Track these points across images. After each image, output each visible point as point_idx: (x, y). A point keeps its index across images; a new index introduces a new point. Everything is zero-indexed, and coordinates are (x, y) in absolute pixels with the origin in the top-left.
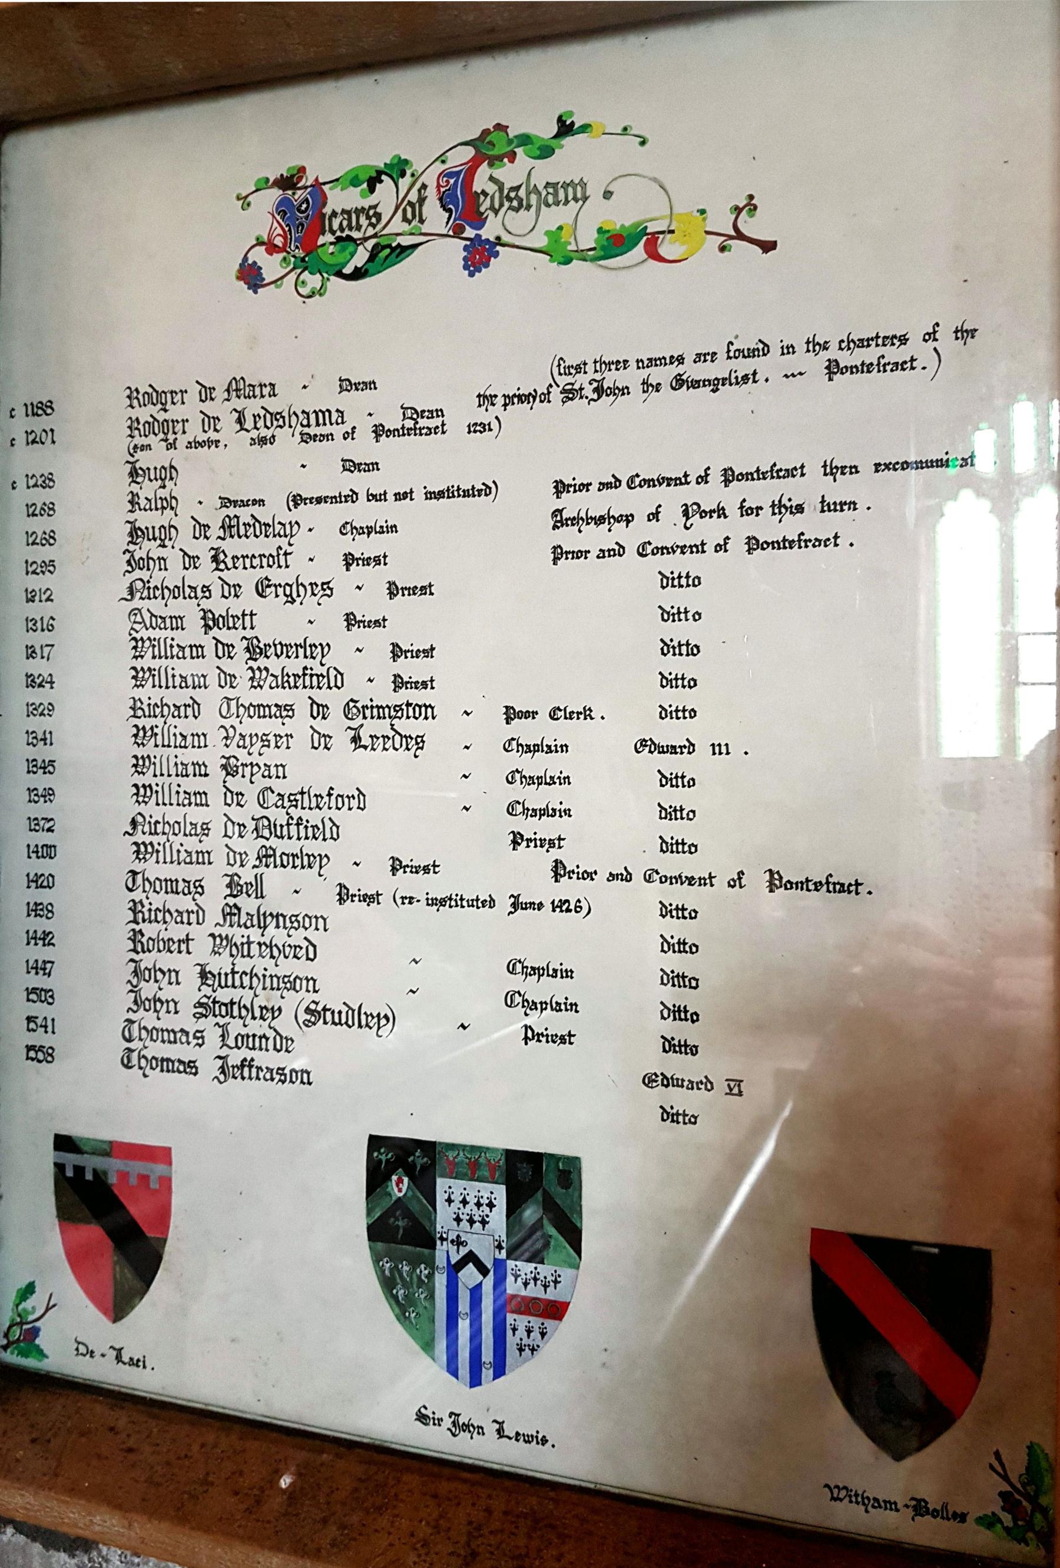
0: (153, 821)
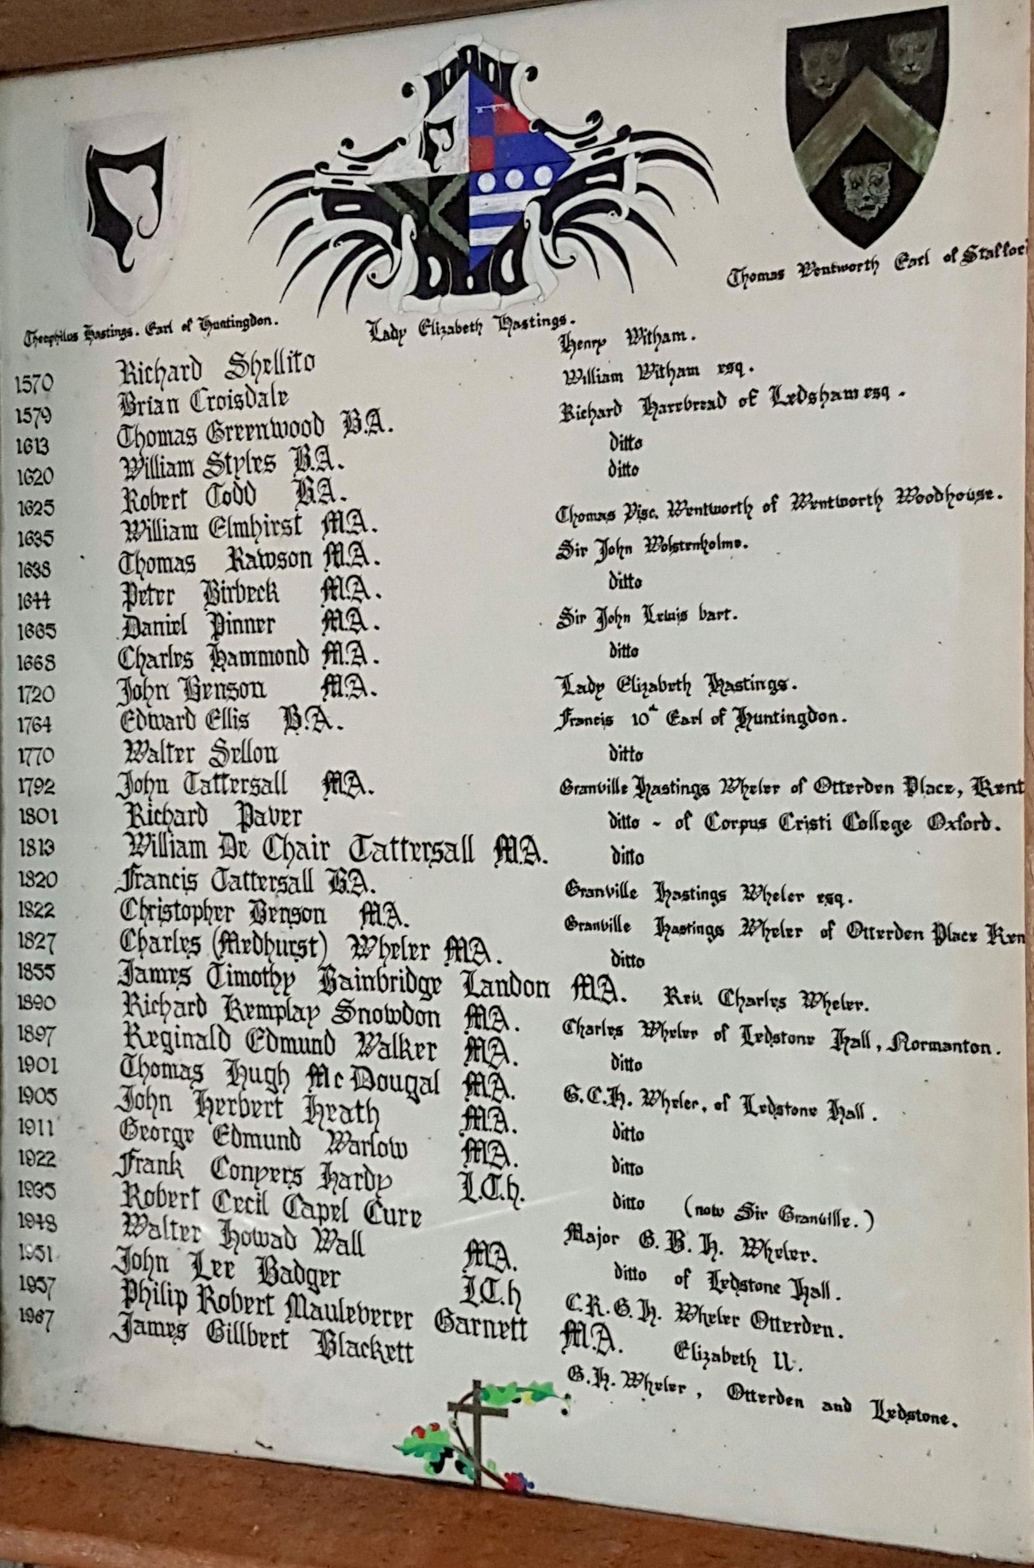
0: (143, 368)
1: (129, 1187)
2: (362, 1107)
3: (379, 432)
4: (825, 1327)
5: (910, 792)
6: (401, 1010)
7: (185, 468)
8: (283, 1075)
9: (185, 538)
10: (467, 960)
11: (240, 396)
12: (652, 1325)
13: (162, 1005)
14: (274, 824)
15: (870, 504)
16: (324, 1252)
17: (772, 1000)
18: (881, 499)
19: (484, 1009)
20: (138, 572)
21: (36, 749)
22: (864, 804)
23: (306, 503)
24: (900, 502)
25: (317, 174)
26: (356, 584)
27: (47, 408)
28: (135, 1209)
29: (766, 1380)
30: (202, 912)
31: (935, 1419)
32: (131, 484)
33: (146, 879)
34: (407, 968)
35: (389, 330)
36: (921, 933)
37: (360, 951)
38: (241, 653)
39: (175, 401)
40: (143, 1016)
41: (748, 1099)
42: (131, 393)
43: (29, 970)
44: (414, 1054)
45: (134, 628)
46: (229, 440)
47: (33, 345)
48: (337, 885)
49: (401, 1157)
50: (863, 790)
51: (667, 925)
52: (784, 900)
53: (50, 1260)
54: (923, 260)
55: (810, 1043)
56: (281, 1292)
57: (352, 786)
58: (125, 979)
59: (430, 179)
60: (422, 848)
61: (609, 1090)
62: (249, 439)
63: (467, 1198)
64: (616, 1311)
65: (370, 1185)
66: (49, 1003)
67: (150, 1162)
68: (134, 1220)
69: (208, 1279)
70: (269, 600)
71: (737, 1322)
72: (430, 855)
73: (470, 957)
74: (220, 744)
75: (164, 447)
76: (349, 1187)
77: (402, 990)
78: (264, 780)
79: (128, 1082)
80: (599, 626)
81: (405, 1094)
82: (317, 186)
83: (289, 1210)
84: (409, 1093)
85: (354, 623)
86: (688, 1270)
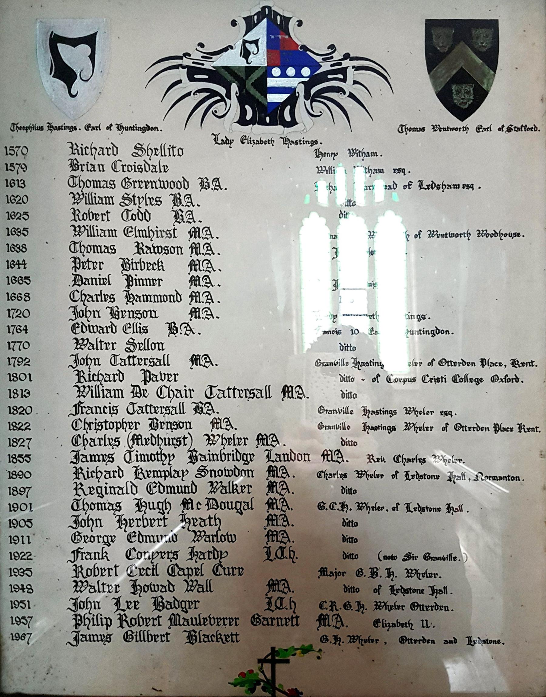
0: (83, 147)
1: (77, 567)
2: (212, 518)
3: (219, 190)
4: (445, 607)
5: (483, 366)
6: (233, 469)
7: (109, 200)
8: (168, 505)
9: (109, 236)
10: (267, 445)
11: (141, 166)
12: (362, 613)
13: (97, 473)
14: (163, 381)
15: (465, 237)
16: (191, 592)
17: (419, 459)
18: (470, 235)
19: (277, 468)
20: (81, 252)
21: (18, 342)
22: (462, 371)
23: (180, 223)
24: (479, 236)
25: (184, 58)
26: (208, 263)
27: (24, 164)
28: (81, 578)
29: (417, 633)
30: (121, 425)
31: (495, 642)
32: (76, 207)
33: (87, 409)
34: (236, 449)
35: (225, 139)
36: (488, 428)
37: (211, 442)
38: (143, 295)
39: (103, 165)
40: (85, 479)
41: (408, 505)
42: (76, 159)
43: (15, 458)
44: (239, 491)
45: (78, 280)
46: (135, 187)
47: (16, 131)
48: (198, 409)
49: (233, 542)
50: (461, 365)
51: (368, 426)
52: (424, 414)
53: (29, 608)
54: (489, 129)
55: (437, 479)
56: (166, 614)
57: (206, 362)
58: (75, 461)
59: (246, 67)
60: (244, 391)
61: (340, 503)
62: (146, 188)
63: (268, 559)
64: (345, 608)
65: (216, 557)
66: (28, 475)
67: (90, 554)
68: (80, 584)
69: (124, 610)
70: (159, 270)
71: (404, 608)
72: (248, 395)
73: (269, 443)
74: (131, 341)
75: (96, 189)
76: (204, 559)
77: (234, 460)
78: (157, 359)
79: (76, 513)
80: (334, 288)
81: (235, 510)
82: (184, 64)
83: (170, 572)
84: (237, 510)
85: (206, 283)
86: (380, 586)
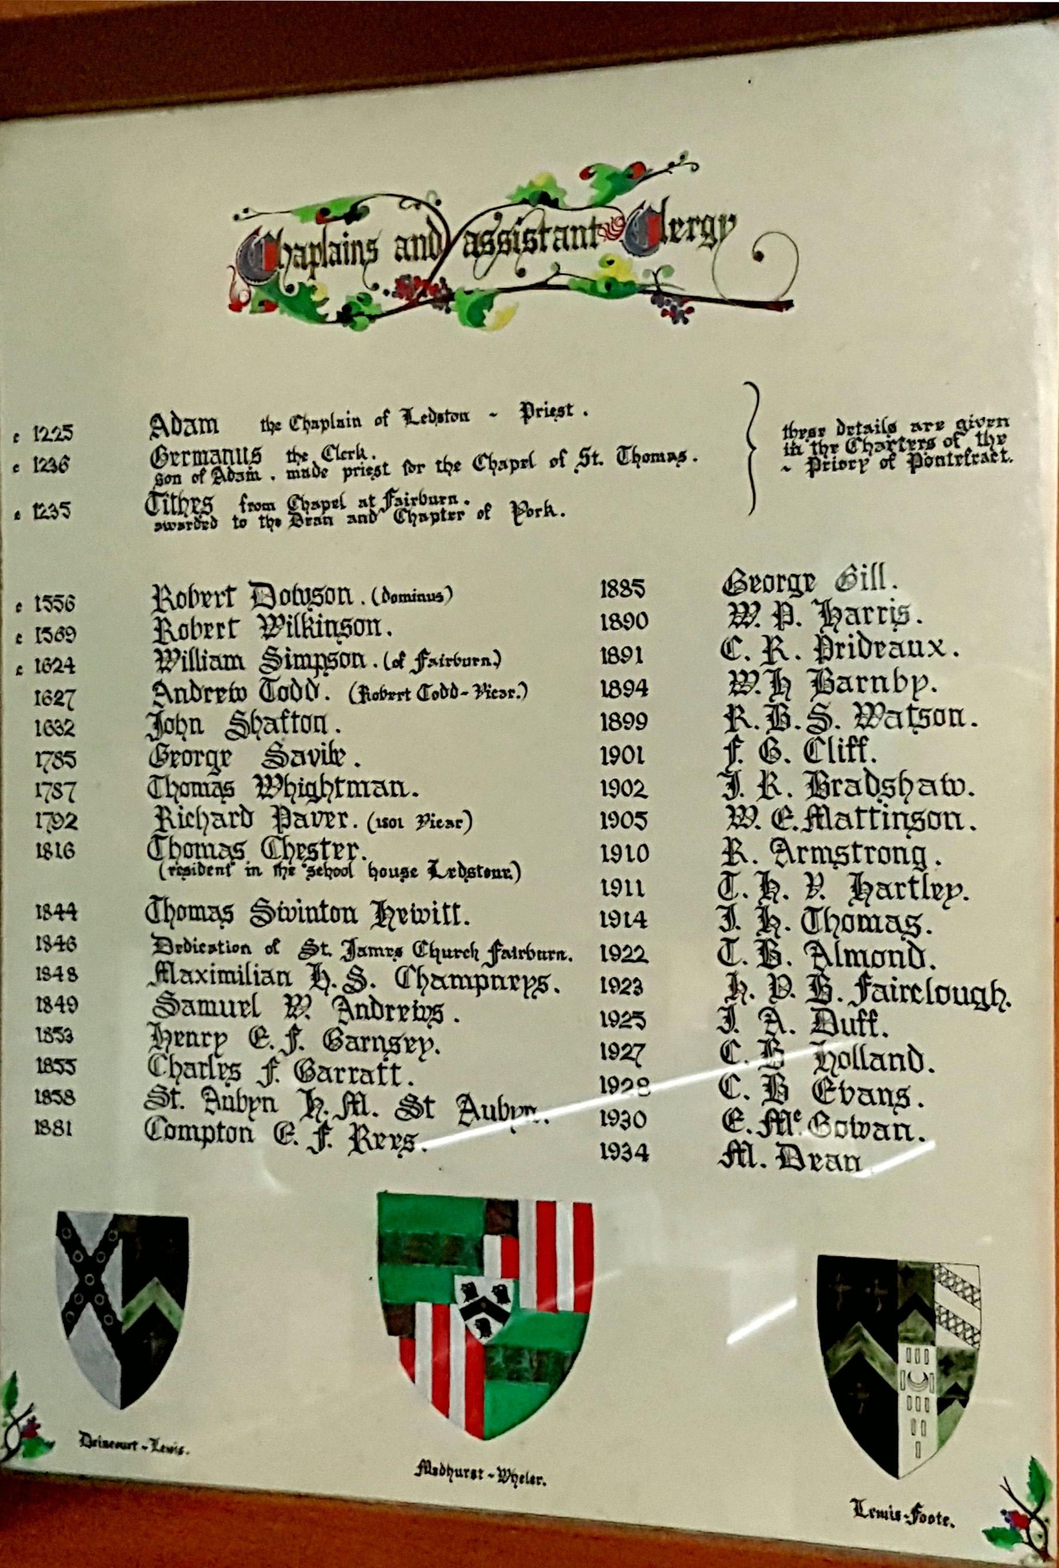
45: (163, 757)
